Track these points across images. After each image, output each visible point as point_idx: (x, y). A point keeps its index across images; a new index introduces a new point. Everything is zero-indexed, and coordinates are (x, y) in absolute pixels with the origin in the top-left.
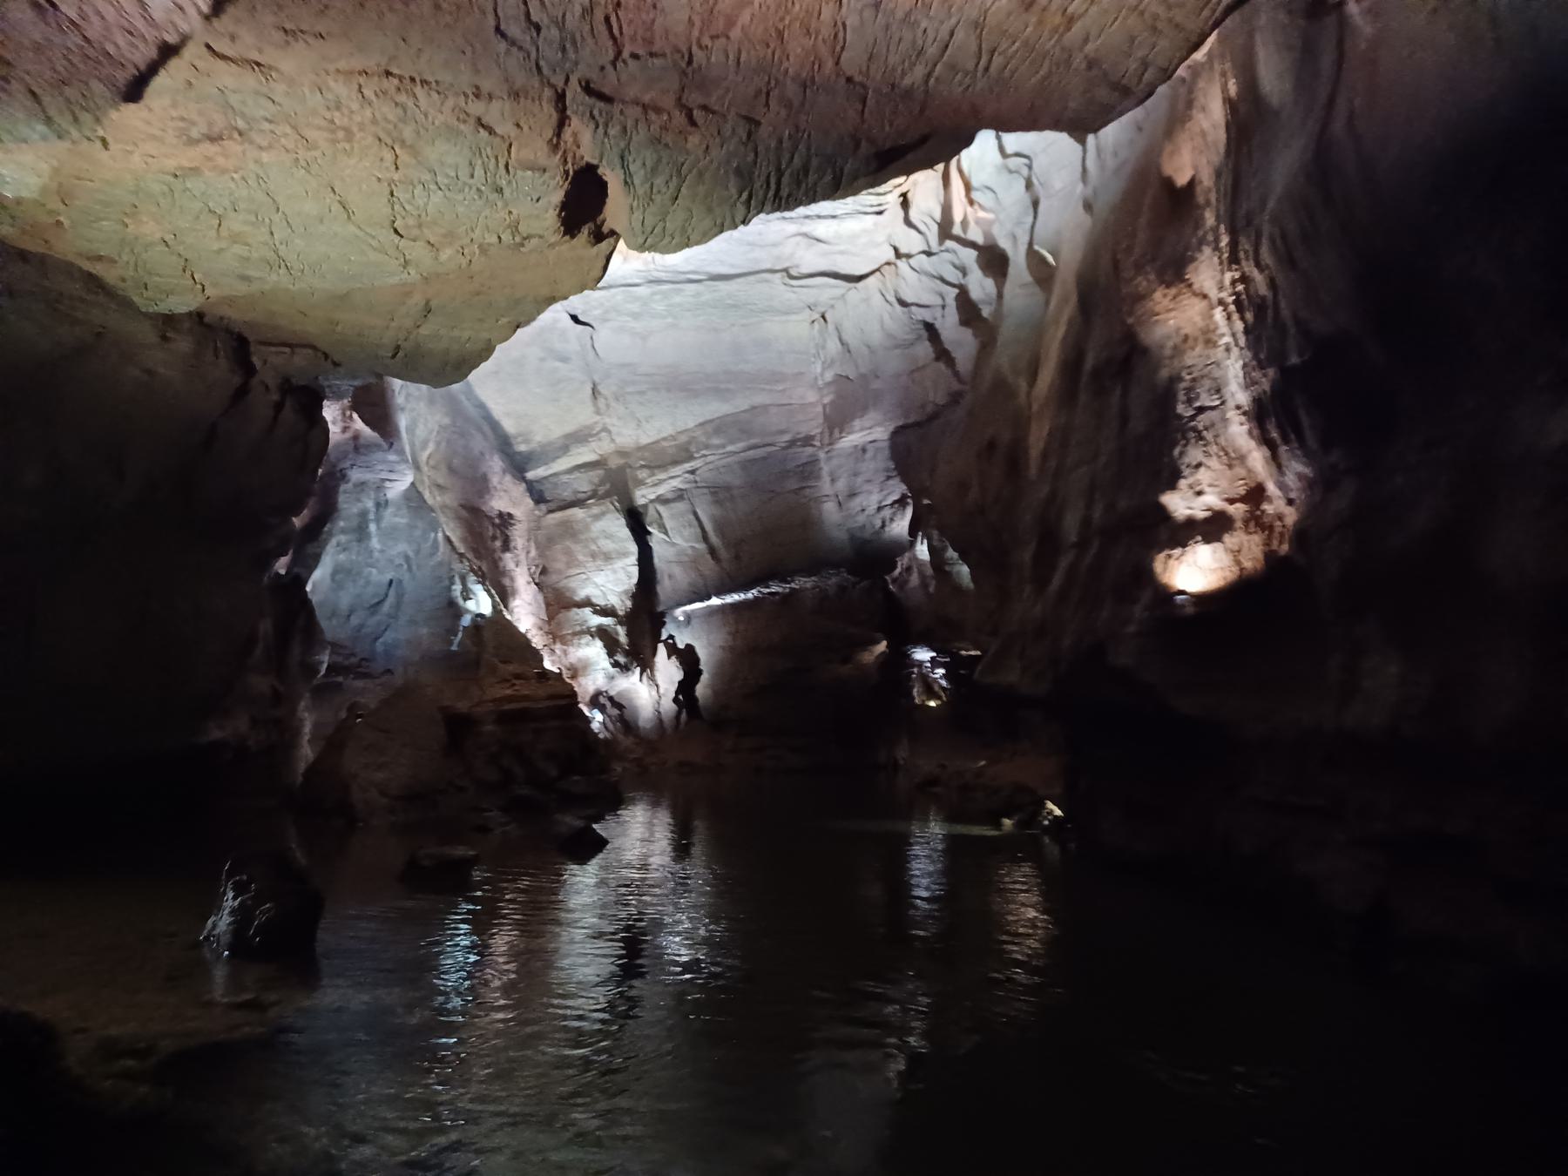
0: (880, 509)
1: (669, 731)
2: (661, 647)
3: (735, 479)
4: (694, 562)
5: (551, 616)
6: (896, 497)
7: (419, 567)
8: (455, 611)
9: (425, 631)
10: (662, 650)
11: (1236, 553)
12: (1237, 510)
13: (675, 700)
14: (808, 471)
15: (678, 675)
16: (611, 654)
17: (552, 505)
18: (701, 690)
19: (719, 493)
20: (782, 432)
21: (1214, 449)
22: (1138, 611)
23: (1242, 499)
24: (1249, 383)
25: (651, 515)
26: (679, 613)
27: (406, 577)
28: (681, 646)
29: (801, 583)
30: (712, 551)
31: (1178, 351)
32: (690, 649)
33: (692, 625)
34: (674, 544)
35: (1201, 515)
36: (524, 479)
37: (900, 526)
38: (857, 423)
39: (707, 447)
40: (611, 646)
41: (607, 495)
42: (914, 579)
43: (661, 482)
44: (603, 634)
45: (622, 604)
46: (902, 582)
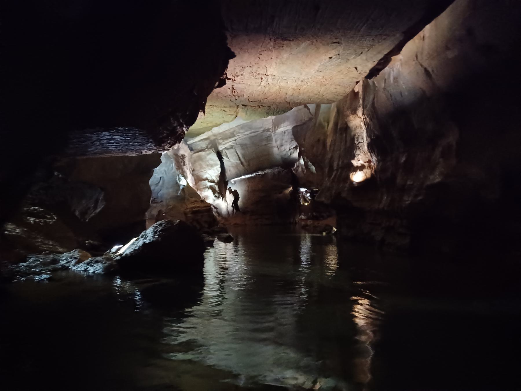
0: (289, 150)
1: (231, 215)
2: (227, 191)
3: (247, 142)
4: (237, 166)
5: (196, 184)
6: (294, 146)
7: (169, 173)
8: (179, 186)
9: (171, 190)
10: (228, 192)
11: (365, 174)
12: (366, 164)
13: (232, 206)
14: (269, 139)
15: (233, 199)
16: (214, 194)
17: (195, 151)
18: (239, 203)
19: (243, 146)
20: (261, 128)
21: (362, 151)
22: (347, 185)
23: (367, 162)
24: (367, 140)
25: (223, 154)
26: (232, 181)
27: (165, 176)
28: (233, 190)
29: (267, 171)
30: (242, 163)
31: (355, 129)
32: (236, 191)
33: (236, 184)
34: (231, 161)
35: (359, 165)
36: (187, 144)
37: (296, 155)
38: (282, 125)
39: (239, 133)
40: (214, 191)
41: (211, 148)
42: (300, 170)
43: (226, 143)
44: (211, 188)
45: (217, 179)
46: (297, 170)
